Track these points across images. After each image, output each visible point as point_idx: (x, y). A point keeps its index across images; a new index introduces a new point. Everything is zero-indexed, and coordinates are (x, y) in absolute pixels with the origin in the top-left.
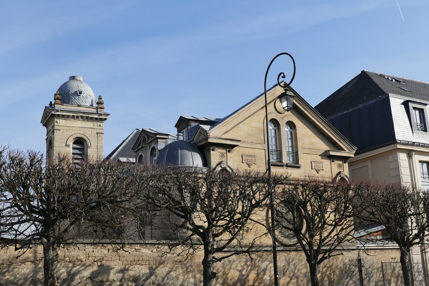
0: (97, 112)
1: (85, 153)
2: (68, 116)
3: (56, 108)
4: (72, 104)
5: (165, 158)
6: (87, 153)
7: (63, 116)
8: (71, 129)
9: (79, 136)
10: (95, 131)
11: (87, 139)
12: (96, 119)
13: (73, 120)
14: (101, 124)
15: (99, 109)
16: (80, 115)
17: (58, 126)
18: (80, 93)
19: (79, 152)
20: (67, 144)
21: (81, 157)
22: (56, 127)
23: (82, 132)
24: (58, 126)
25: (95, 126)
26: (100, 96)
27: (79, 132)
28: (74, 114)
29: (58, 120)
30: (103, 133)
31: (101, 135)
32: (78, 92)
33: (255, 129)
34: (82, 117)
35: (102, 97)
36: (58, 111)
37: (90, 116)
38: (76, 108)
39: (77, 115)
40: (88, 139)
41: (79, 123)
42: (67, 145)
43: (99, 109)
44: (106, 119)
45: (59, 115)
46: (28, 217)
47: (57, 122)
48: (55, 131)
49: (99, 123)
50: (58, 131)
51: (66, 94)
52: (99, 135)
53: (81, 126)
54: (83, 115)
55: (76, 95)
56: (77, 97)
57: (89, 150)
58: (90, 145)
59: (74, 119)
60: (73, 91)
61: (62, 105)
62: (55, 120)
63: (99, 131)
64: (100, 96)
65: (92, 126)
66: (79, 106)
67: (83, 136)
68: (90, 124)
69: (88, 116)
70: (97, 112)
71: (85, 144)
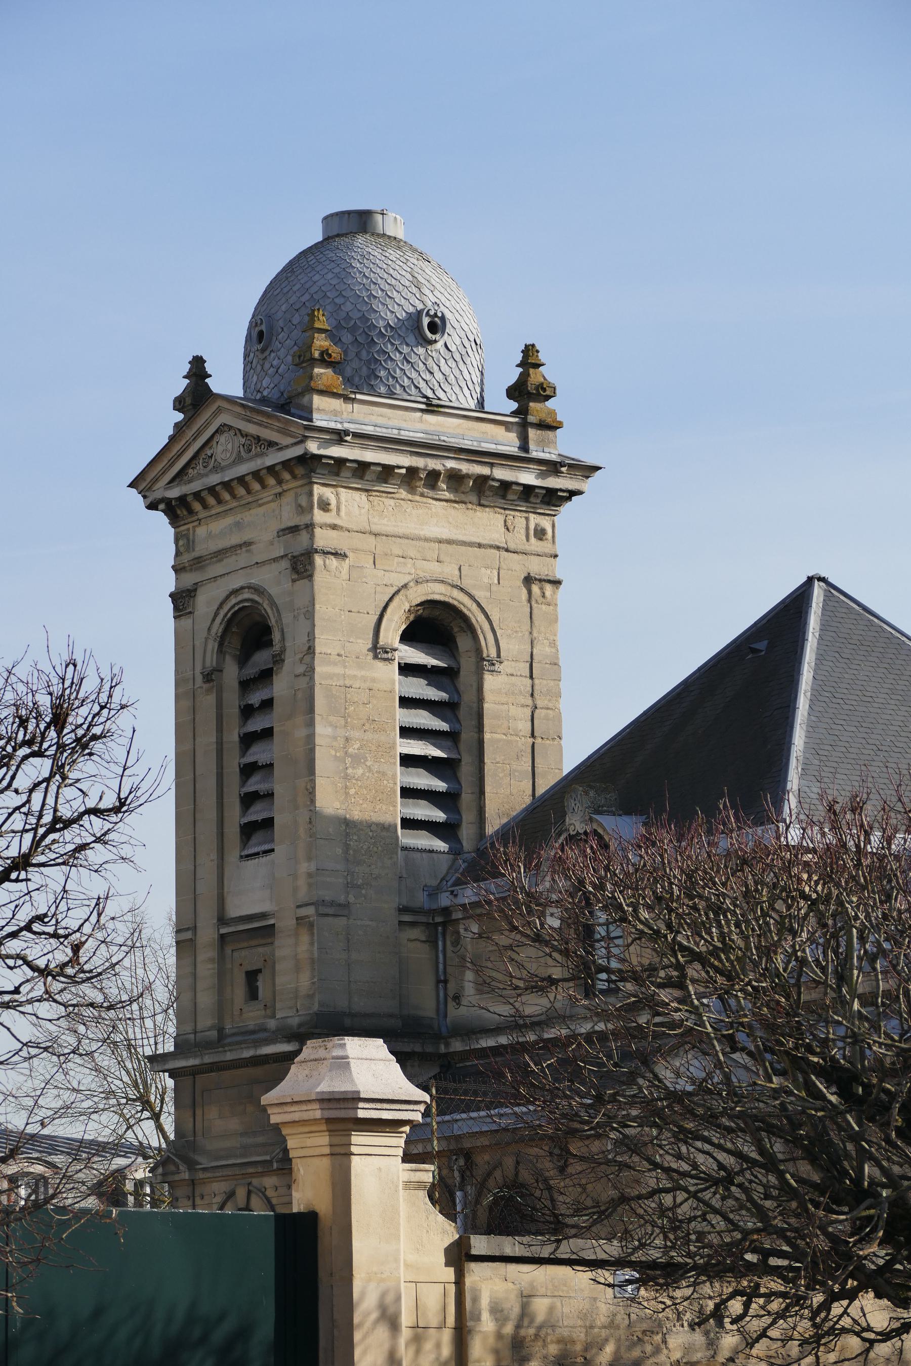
0: (524, 447)
1: (468, 697)
2: (387, 472)
3: (319, 420)
4: (391, 395)
5: (363, 673)
6: (480, 699)
7: (362, 467)
8: (396, 548)
9: (439, 592)
10: (517, 567)
11: (477, 618)
12: (528, 490)
13: (403, 493)
14: (545, 523)
15: (532, 433)
16: (451, 464)
17: (334, 527)
18: (433, 328)
19: (433, 694)
20: (382, 642)
21: (443, 726)
22: (323, 538)
23: (449, 571)
24: (334, 527)
25: (517, 539)
26: (529, 351)
27: (434, 568)
28: (419, 462)
29: (328, 493)
30: (557, 583)
31: (548, 588)
32: (426, 321)
33: (318, 471)
34: (455, 478)
35: (542, 357)
36: (339, 436)
37: (501, 474)
38: (417, 425)
39: (433, 464)
40: (481, 618)
41: (437, 518)
42: (378, 651)
43: (532, 433)
44: (573, 493)
45: (341, 462)
46: (830, 1283)
47: (325, 506)
48: (318, 560)
49: (534, 519)
50: (333, 562)
51: (353, 330)
52: (535, 588)
53: (445, 534)
54: (465, 468)
55: (411, 339)
56: (421, 351)
57: (490, 682)
58: (493, 653)
59: (412, 490)
60: (396, 307)
61: (347, 399)
62: (317, 490)
63: (536, 567)
64: (529, 351)
65: (497, 535)
66: (432, 407)
67: (456, 593)
68: (487, 524)
69: (485, 471)
70: (524, 447)
71: (463, 642)
